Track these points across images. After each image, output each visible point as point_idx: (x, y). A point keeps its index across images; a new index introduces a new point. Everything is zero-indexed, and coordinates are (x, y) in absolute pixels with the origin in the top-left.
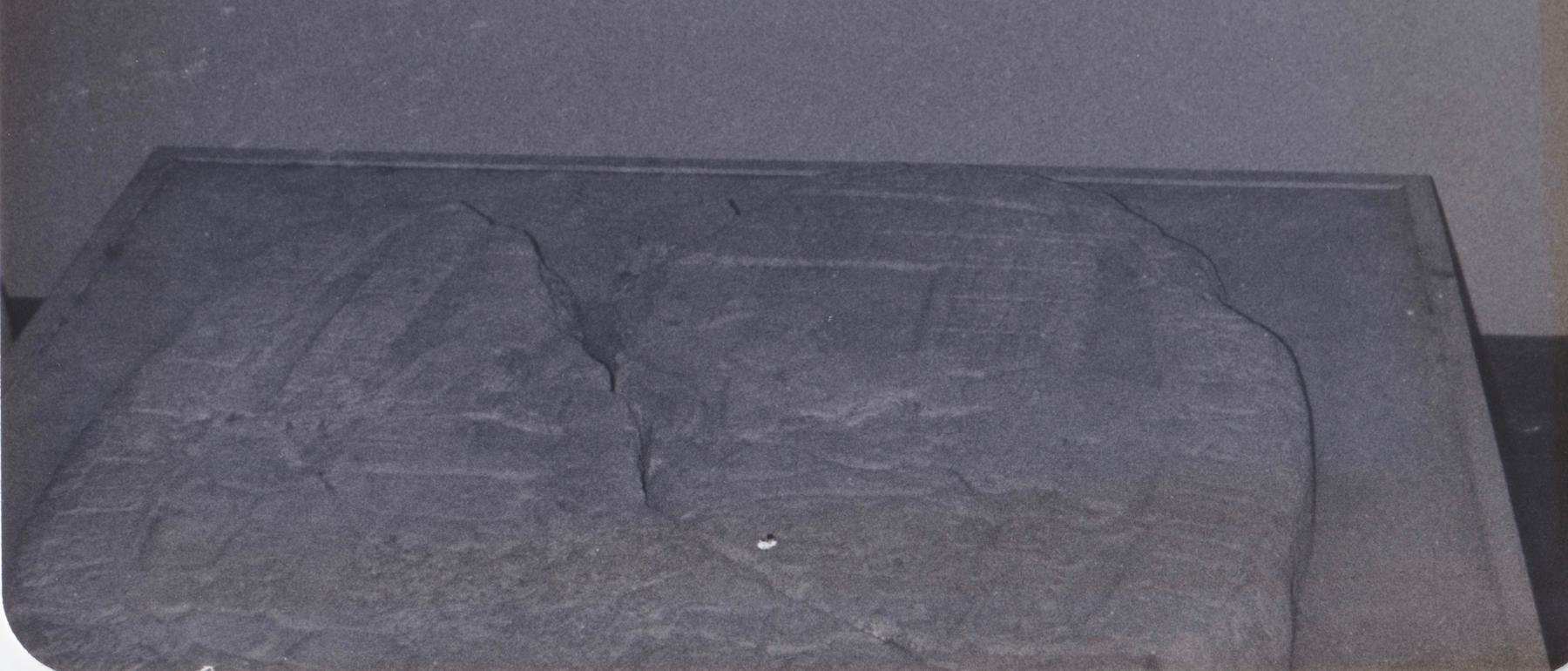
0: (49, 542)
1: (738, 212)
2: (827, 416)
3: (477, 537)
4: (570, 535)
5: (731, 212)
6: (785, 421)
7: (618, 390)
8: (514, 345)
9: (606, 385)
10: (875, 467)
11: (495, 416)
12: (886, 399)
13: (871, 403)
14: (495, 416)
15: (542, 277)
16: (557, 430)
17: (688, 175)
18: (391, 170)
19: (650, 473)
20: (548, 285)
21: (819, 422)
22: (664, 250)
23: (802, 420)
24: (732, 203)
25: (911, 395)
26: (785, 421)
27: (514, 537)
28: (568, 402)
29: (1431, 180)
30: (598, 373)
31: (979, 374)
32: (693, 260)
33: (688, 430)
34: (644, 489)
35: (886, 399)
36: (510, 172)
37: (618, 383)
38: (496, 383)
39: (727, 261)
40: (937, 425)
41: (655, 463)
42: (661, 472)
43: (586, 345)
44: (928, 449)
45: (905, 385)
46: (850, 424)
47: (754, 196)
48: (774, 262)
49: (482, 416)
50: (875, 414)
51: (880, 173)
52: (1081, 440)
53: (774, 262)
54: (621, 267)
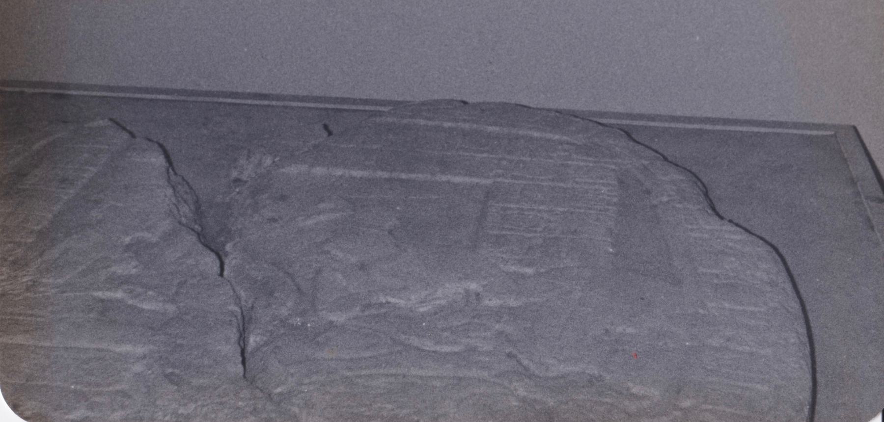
0: (252, 327)
1: (330, 133)
2: (402, 302)
3: (91, 407)
4: (174, 406)
5: (325, 134)
6: (369, 306)
7: (226, 273)
8: (139, 234)
9: (216, 269)
10: (446, 349)
11: (119, 295)
12: (450, 290)
13: (439, 293)
14: (119, 295)
15: (169, 180)
16: (171, 308)
17: (277, 107)
18: (61, 96)
19: (249, 349)
20: (173, 188)
21: (395, 307)
22: (268, 161)
23: (381, 305)
24: (326, 127)
25: (473, 286)
26: (369, 306)
27: (123, 407)
28: (181, 285)
29: (855, 128)
30: (210, 261)
31: (529, 271)
32: (293, 170)
33: (284, 312)
34: (244, 362)
35: (450, 290)
36: (151, 100)
37: (226, 267)
38: (130, 268)
39: (319, 171)
40: (498, 314)
41: (253, 340)
42: (257, 349)
43: (201, 236)
44: (488, 334)
45: (467, 277)
46: (422, 310)
47: (336, 122)
48: (357, 173)
49: (108, 295)
50: (443, 302)
51: (433, 107)
52: (620, 329)
53: (357, 173)
54: (234, 174)
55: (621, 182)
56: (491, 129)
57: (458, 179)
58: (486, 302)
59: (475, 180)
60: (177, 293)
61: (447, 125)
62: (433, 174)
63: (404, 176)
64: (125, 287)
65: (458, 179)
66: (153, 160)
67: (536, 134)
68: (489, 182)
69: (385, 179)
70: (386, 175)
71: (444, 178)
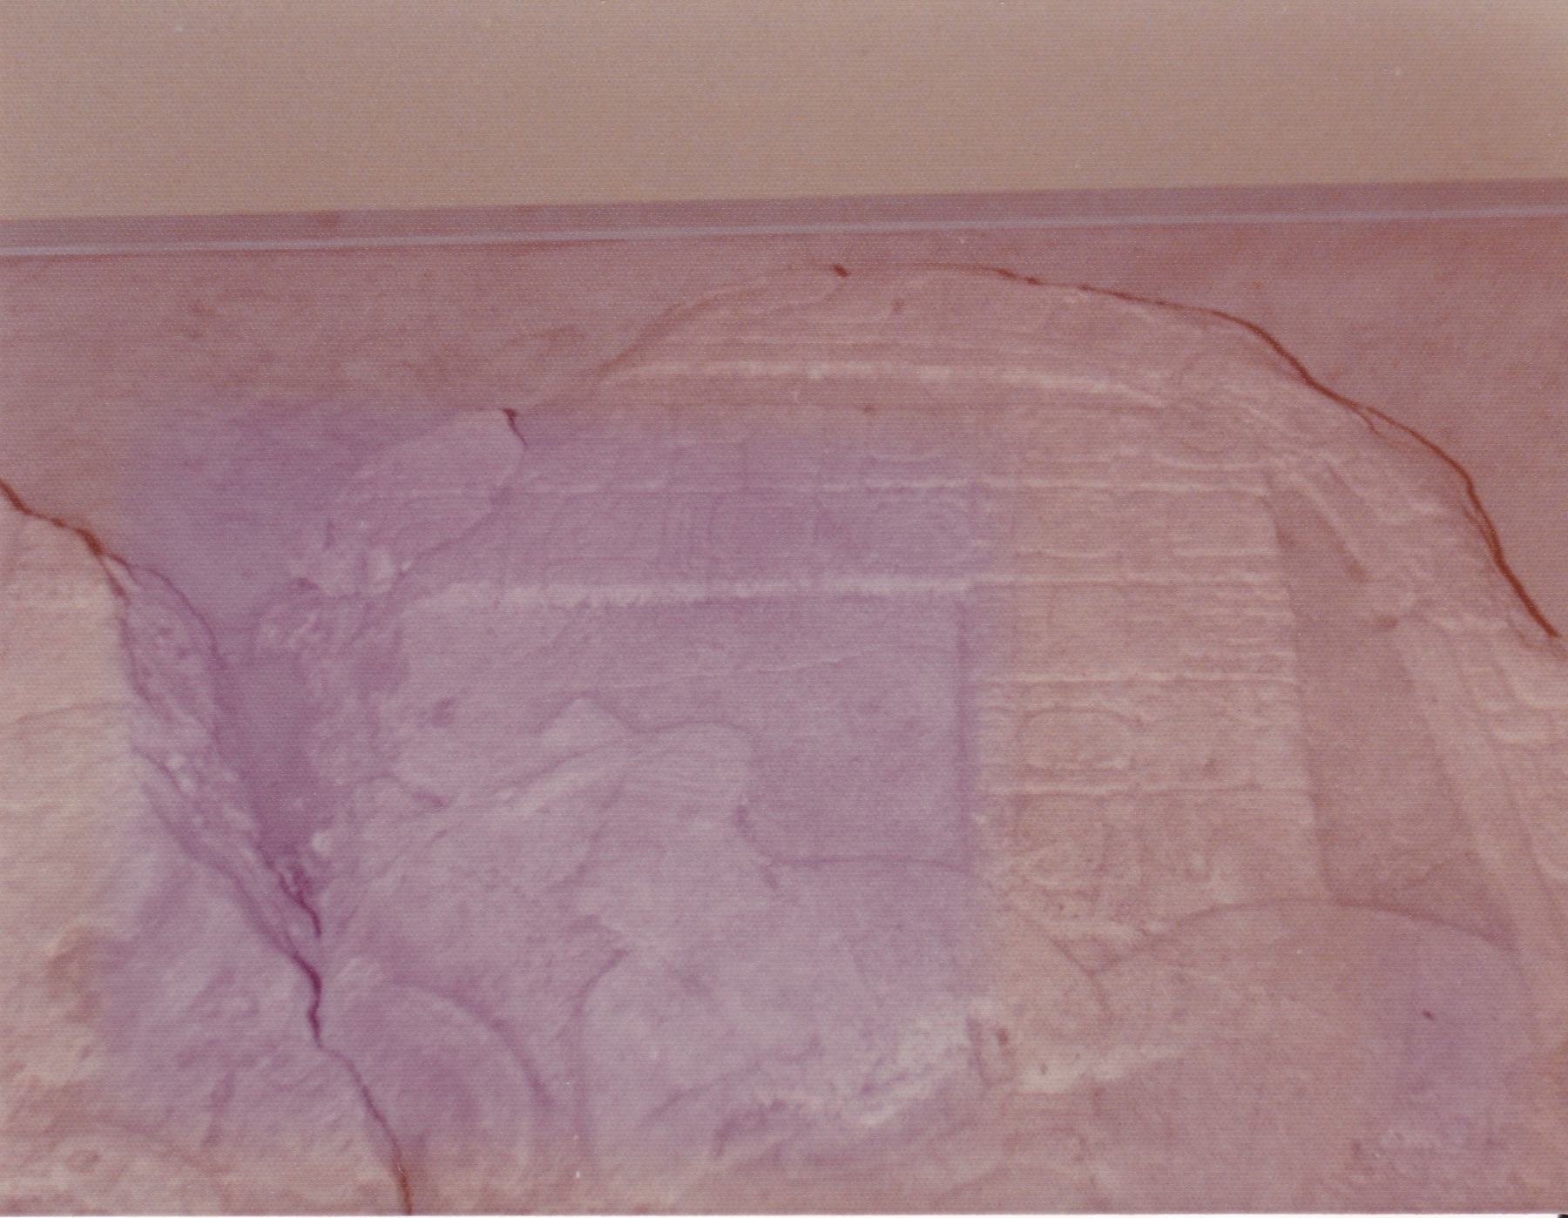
8: (82, 920)
22: (384, 567)
28: (220, 1101)
53: (626, 593)
54: (297, 569)
55: (1284, 539)
56: (931, 373)
57: (882, 585)
58: (1033, 1081)
59: (923, 584)
60: (212, 1138)
61: (817, 371)
62: (977, 588)
63: (741, 590)
64: (67, 1149)
65: (882, 585)
66: (81, 603)
67: (1047, 381)
68: (961, 585)
69: (697, 605)
70: (691, 591)
71: (847, 583)
